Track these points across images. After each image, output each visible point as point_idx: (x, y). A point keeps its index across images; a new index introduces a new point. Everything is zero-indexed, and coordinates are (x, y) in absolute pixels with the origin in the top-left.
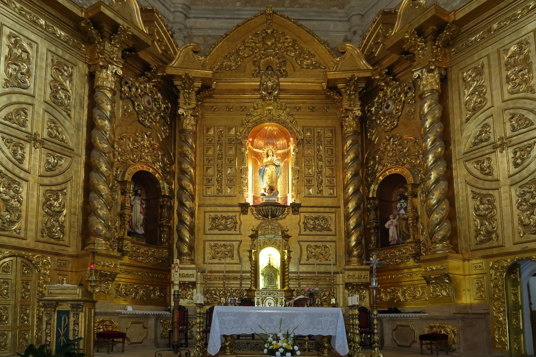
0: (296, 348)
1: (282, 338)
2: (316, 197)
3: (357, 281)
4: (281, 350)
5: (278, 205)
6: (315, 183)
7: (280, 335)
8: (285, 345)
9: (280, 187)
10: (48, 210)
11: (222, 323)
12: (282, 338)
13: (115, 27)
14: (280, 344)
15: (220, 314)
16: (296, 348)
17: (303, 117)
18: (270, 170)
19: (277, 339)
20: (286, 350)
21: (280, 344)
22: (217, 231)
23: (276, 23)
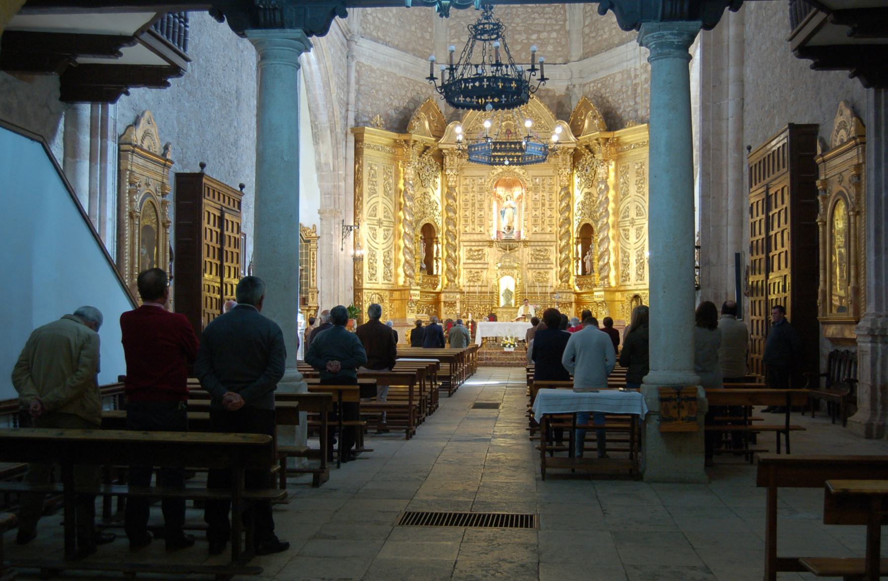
0: (516, 343)
1: (509, 339)
2: (541, 234)
3: (564, 300)
4: (509, 344)
5: (513, 241)
6: (540, 222)
7: (509, 337)
8: (510, 342)
9: (515, 225)
10: (411, 272)
11: (482, 331)
12: (509, 339)
13: (826, 185)
14: (508, 341)
15: (481, 326)
16: (516, 343)
17: (852, 259)
18: (509, 212)
19: (507, 339)
20: (511, 344)
21: (508, 341)
22: (471, 261)
23: (519, 64)
